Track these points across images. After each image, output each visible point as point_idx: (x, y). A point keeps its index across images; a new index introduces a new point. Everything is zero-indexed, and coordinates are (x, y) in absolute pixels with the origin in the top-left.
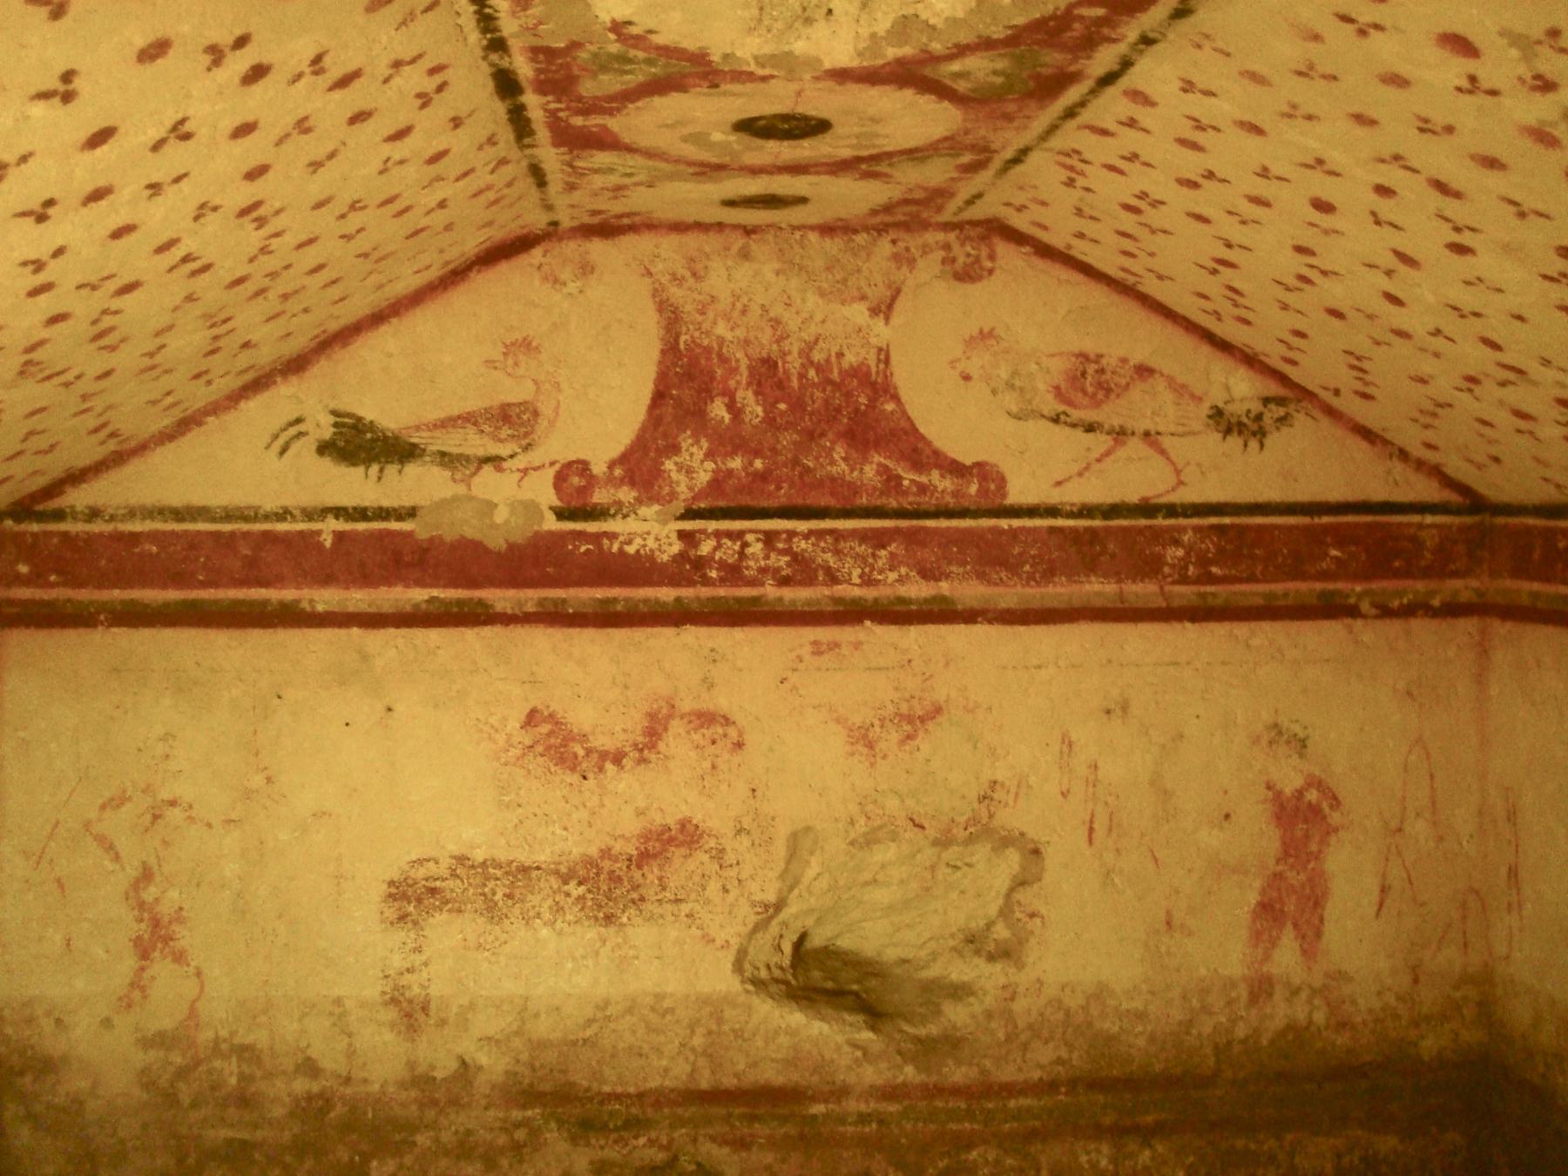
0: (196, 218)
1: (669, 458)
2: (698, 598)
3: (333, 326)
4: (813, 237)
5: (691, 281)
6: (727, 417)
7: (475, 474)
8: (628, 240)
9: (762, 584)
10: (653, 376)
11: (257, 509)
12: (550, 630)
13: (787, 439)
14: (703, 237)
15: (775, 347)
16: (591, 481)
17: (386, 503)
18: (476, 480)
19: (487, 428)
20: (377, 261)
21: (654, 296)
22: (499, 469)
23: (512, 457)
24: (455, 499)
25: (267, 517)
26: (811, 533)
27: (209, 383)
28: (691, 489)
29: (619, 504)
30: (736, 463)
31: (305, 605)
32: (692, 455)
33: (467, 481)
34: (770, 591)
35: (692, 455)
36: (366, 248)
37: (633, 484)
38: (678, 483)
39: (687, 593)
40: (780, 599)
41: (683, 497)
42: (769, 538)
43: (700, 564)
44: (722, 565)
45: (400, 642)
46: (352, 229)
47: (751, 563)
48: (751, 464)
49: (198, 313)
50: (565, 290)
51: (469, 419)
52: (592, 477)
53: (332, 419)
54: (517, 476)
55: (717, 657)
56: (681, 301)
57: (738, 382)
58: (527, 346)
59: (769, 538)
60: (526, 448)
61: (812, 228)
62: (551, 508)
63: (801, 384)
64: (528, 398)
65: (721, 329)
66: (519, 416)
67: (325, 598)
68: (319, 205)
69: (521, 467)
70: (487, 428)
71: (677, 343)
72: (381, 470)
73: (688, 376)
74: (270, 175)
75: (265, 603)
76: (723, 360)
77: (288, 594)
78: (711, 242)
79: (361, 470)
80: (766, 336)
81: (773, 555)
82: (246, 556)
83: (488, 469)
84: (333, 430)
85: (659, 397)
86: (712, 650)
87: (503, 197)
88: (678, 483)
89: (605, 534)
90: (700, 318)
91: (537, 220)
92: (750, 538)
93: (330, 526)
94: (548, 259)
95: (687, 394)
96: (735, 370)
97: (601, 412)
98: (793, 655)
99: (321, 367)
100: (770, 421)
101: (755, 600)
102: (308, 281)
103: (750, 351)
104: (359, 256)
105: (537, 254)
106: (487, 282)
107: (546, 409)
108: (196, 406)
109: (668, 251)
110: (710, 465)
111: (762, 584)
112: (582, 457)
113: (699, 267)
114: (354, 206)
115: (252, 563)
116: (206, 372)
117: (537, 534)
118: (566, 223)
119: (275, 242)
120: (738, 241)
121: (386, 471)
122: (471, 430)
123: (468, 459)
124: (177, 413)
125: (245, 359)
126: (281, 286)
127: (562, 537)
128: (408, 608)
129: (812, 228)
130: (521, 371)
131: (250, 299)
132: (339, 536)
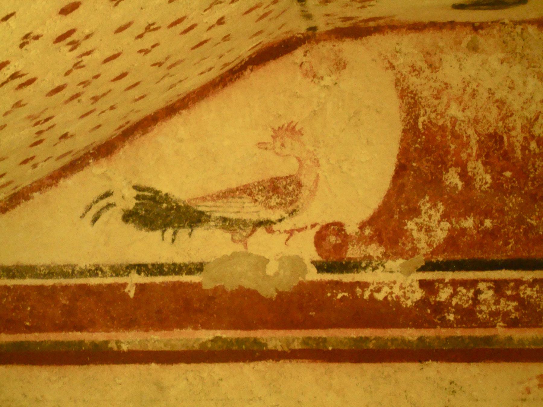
0: (22, 46)
1: (411, 219)
2: (438, 338)
3: (135, 118)
4: (532, 29)
5: (428, 72)
6: (460, 184)
7: (250, 235)
8: (374, 40)
9: (494, 326)
10: (396, 152)
11: (74, 267)
12: (313, 365)
13: (513, 201)
14: (438, 34)
15: (500, 124)
16: (346, 239)
17: (179, 260)
18: (251, 240)
19: (260, 198)
20: (169, 68)
21: (396, 85)
22: (270, 231)
23: (280, 221)
24: (235, 255)
25: (82, 273)
26: (535, 281)
27: (35, 166)
28: (430, 245)
29: (370, 258)
30: (469, 223)
31: (113, 345)
32: (430, 217)
33: (244, 241)
34: (501, 331)
35: (430, 217)
36: (159, 59)
37: (381, 242)
38: (419, 240)
39: (429, 333)
40: (510, 339)
41: (423, 252)
42: (499, 287)
43: (440, 308)
44: (458, 310)
45: (190, 375)
46: (148, 46)
47: (484, 308)
48: (482, 223)
49: (25, 115)
50: (322, 83)
51: (246, 191)
52: (346, 236)
53: (135, 193)
54: (286, 236)
55: (456, 389)
56: (419, 88)
57: (469, 155)
58: (292, 130)
59: (499, 287)
60: (292, 213)
61: (531, 22)
62: (313, 262)
63: (524, 155)
64: (293, 173)
65: (454, 111)
66: (285, 188)
67: (129, 339)
68: (121, 29)
69: (288, 229)
70: (260, 198)
71: (416, 123)
72: (175, 233)
73: (426, 150)
74: (81, 10)
75: (81, 343)
76: (456, 136)
77: (99, 336)
78: (444, 38)
79: (159, 233)
80: (493, 115)
81: (502, 301)
82: (65, 305)
83: (261, 231)
84: (135, 201)
85: (401, 169)
86: (452, 383)
87: (270, 12)
88: (419, 240)
89: (358, 283)
90: (436, 102)
91: (300, 27)
92: (482, 286)
93: (135, 278)
94: (308, 58)
95: (425, 166)
96: (467, 145)
97: (353, 181)
98: (521, 388)
99: (125, 152)
100: (497, 186)
101: (487, 340)
102: (113, 85)
103: (479, 128)
104: (154, 65)
105: (299, 54)
106: (256, 78)
107: (307, 181)
108: (24, 185)
109: (407, 48)
110: (446, 225)
111: (494, 326)
112: (337, 219)
113: (435, 59)
114: (149, 28)
115: (69, 311)
116: (32, 158)
117: (301, 284)
118: (322, 28)
119: (86, 59)
120: (467, 37)
121: (178, 234)
122: (247, 200)
123: (244, 223)
124: (9, 191)
125: (63, 147)
126: (91, 92)
127: (322, 286)
128: (197, 347)
129: (531, 22)
130: (286, 151)
131: (67, 102)
132: (141, 288)
